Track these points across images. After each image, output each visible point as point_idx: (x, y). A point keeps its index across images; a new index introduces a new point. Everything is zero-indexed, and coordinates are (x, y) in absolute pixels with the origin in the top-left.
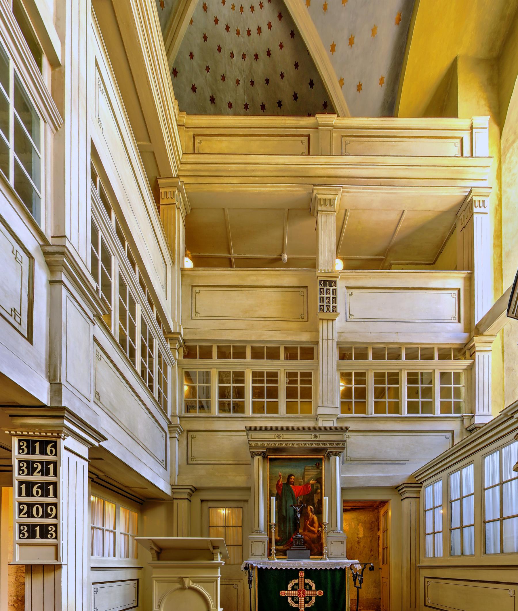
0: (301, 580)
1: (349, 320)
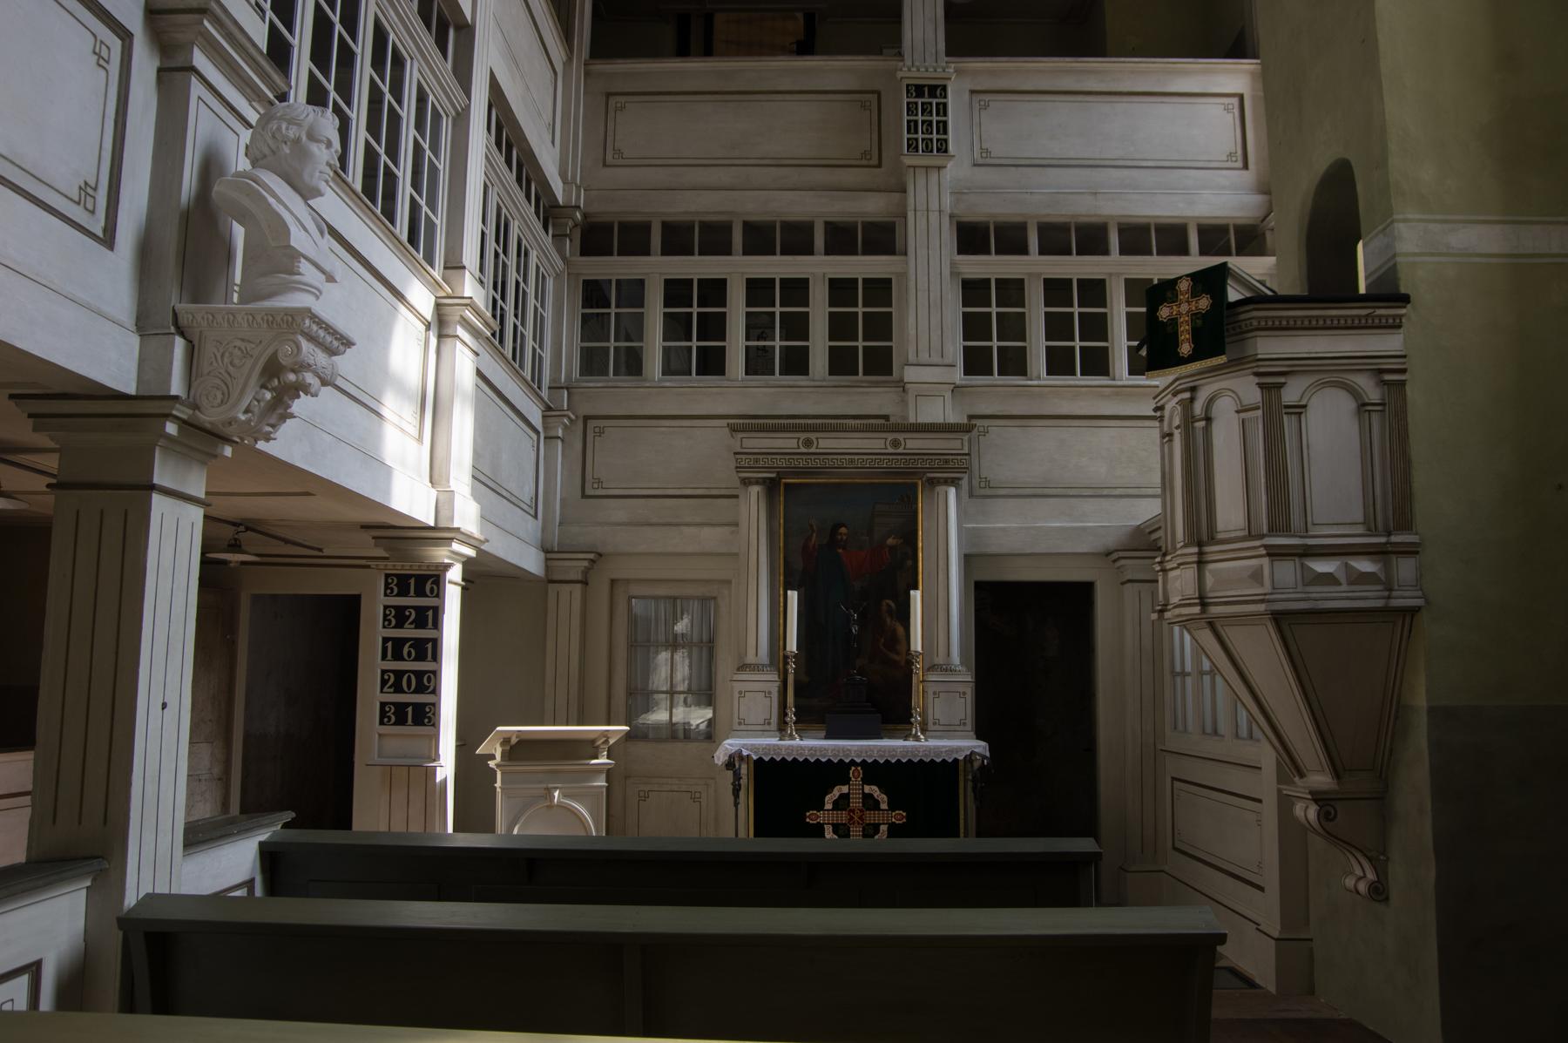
0: (855, 788)
1: (981, 161)
